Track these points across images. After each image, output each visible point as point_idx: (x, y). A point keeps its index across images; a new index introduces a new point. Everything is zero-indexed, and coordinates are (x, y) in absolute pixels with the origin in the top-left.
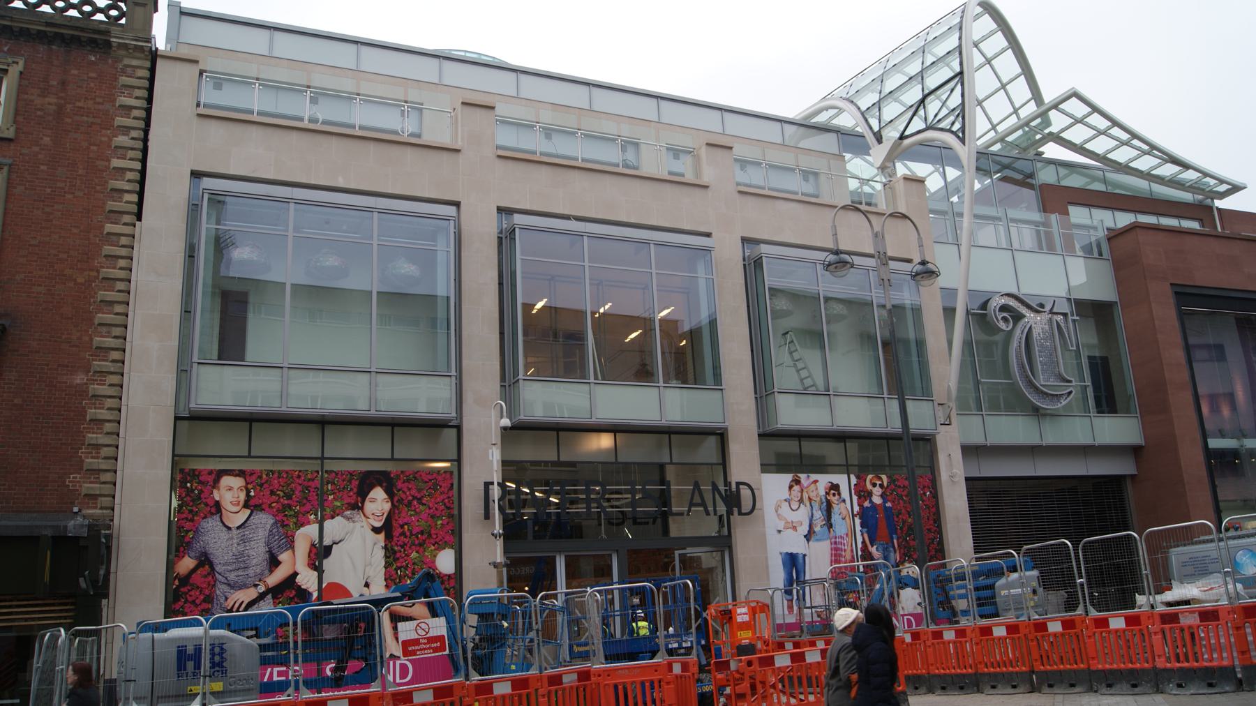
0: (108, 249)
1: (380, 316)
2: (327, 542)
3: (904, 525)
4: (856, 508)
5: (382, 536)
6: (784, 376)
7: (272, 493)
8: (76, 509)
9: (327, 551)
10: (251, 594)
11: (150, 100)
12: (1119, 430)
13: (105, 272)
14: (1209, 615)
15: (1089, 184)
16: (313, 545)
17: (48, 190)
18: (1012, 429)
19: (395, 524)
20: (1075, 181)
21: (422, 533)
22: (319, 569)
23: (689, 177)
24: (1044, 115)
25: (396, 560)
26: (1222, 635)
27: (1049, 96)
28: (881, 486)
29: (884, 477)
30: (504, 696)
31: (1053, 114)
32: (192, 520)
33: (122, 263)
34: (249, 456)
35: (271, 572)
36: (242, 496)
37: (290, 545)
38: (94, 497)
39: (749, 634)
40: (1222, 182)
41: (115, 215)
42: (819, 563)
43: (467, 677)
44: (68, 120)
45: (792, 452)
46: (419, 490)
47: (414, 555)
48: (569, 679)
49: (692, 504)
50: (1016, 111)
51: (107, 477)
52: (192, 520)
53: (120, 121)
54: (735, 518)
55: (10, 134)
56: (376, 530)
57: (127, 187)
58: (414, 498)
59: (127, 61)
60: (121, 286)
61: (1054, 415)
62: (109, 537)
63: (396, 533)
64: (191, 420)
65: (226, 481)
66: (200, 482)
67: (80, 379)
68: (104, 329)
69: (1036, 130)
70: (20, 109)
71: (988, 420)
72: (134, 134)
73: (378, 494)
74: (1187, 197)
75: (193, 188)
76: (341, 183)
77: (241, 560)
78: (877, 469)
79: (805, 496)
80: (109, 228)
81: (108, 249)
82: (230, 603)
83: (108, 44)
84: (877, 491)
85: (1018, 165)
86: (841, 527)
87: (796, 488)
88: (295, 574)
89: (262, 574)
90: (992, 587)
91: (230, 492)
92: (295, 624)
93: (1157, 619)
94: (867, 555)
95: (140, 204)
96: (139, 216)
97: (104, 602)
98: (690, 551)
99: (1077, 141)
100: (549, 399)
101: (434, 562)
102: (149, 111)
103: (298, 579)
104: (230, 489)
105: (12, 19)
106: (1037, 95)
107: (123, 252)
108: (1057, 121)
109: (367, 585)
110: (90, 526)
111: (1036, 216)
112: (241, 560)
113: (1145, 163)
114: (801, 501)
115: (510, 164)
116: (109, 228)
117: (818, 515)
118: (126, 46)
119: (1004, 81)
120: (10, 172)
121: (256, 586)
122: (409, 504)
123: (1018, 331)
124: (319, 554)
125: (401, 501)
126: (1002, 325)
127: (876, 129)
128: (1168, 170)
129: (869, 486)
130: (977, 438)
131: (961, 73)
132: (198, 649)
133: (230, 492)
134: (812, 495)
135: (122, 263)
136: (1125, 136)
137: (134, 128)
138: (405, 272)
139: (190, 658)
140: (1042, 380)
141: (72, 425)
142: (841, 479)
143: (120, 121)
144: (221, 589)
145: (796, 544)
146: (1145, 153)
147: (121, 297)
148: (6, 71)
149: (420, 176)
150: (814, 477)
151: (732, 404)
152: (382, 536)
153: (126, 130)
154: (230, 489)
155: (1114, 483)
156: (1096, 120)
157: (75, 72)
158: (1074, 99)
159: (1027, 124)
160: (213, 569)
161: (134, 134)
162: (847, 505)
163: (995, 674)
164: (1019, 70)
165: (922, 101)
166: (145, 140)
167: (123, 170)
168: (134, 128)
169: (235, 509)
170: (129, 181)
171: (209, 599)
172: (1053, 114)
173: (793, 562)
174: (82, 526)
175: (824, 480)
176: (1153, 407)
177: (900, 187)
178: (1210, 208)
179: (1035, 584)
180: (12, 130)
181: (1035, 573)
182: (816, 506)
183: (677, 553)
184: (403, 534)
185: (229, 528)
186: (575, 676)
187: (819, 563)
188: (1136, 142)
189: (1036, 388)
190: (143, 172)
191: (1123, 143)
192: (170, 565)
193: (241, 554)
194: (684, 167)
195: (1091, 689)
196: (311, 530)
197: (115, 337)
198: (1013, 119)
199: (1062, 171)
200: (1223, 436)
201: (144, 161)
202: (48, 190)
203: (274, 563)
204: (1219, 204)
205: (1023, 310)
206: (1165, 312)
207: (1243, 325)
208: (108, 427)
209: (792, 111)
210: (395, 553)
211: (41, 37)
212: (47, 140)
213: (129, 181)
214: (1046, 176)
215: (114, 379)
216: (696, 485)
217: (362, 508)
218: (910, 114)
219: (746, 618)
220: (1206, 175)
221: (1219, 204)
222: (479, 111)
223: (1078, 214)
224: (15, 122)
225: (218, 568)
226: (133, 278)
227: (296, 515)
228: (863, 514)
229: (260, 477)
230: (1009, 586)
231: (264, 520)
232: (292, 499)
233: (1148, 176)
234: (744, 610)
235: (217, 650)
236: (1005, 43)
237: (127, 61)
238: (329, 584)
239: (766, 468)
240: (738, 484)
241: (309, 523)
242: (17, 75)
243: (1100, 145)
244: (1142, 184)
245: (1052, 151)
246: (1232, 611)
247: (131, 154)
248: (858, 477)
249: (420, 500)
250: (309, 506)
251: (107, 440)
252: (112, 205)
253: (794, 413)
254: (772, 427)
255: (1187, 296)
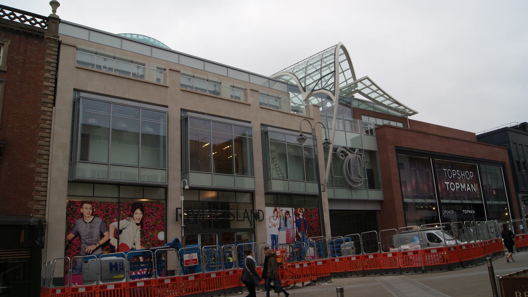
0: (43, 117)
1: (113, 139)
2: (121, 228)
3: (309, 226)
4: (294, 220)
5: (139, 227)
6: (274, 174)
7: (101, 210)
8: (31, 215)
9: (121, 232)
10: (94, 247)
11: (58, 60)
12: (375, 195)
13: (42, 125)
14: (415, 252)
15: (367, 108)
16: (116, 230)
17: (20, 92)
18: (342, 193)
19: (144, 222)
20: (363, 107)
21: (153, 225)
22: (118, 238)
23: (242, 100)
24: (356, 85)
25: (144, 235)
26: (419, 258)
27: (358, 78)
28: (302, 212)
29: (303, 209)
30: (214, 278)
31: (359, 84)
32: (73, 220)
33: (48, 122)
34: (93, 196)
35: (101, 239)
36: (91, 211)
37: (108, 229)
38: (38, 210)
39: (281, 259)
40: (411, 111)
41: (45, 104)
42: (282, 239)
43: (156, 278)
44: (28, 66)
45: (278, 199)
46: (152, 210)
47: (150, 233)
48: (231, 273)
49: (244, 217)
50: (346, 81)
51: (43, 203)
52: (73, 220)
53: (47, 67)
54: (257, 222)
55: (5, 69)
56: (137, 224)
57: (50, 93)
58: (151, 213)
59: (49, 44)
60: (47, 131)
61: (356, 189)
62: (45, 225)
63: (144, 226)
64: (73, 182)
65: (85, 205)
66: (76, 206)
67: (32, 165)
68: (41, 147)
69: (352, 88)
70: (9, 60)
71: (307, 184)
72: (52, 73)
73: (138, 211)
74: (399, 114)
75: (75, 95)
76: (127, 96)
77: (91, 235)
78: (301, 206)
79: (279, 215)
80: (43, 108)
81: (43, 117)
82: (87, 250)
83: (43, 37)
84: (301, 214)
85: (345, 99)
86: (289, 226)
87: (276, 212)
88: (110, 240)
89: (98, 240)
90: (339, 247)
91: (86, 209)
92: (154, 255)
93: (401, 254)
94: (297, 236)
95: (54, 100)
96: (54, 104)
97: (43, 249)
98: (238, 233)
99: (366, 93)
100: (199, 179)
101: (157, 236)
102: (57, 64)
103: (111, 242)
104: (87, 208)
105: (7, 24)
106: (354, 76)
107: (48, 118)
108: (360, 86)
109: (134, 244)
110: (39, 222)
111: (351, 119)
112: (91, 235)
113: (387, 103)
114: (277, 217)
115: (185, 93)
116: (43, 108)
117: (282, 221)
118: (49, 39)
119: (344, 70)
120: (5, 84)
121: (96, 244)
122: (149, 215)
123: (346, 160)
124: (118, 233)
125: (146, 214)
126: (341, 157)
127: (303, 86)
128: (395, 105)
129: (299, 212)
130: (332, 197)
131: (335, 71)
132: (116, 264)
133: (86, 209)
134: (281, 215)
135: (48, 122)
136: (382, 93)
137: (52, 71)
138: (150, 130)
139: (114, 266)
140: (353, 177)
141: (29, 182)
142: (290, 209)
143: (47, 67)
144: (83, 245)
145: (275, 232)
146: (388, 99)
147: (48, 135)
148: (3, 44)
149: (154, 96)
150: (281, 208)
151: (252, 182)
152: (139, 227)
153: (49, 71)
154: (87, 208)
155: (373, 213)
156: (373, 87)
157: (30, 47)
158: (367, 80)
159: (350, 86)
160: (80, 238)
161: (52, 73)
162: (292, 218)
163: (352, 272)
164: (349, 67)
165: (321, 79)
166: (56, 75)
167: (48, 86)
168: (52, 71)
169: (88, 216)
170: (50, 91)
171: (79, 249)
172: (359, 84)
173: (274, 238)
174: (36, 221)
175: (285, 209)
176: (387, 188)
177: (312, 108)
178: (406, 119)
179: (353, 246)
180: (6, 68)
181: (353, 242)
182: (282, 219)
183: (235, 234)
184: (147, 226)
185: (86, 223)
186: (232, 272)
187: (282, 239)
188: (385, 96)
189: (351, 180)
190: (55, 88)
191: (381, 96)
192: (66, 236)
193: (91, 232)
194: (238, 93)
195: (382, 275)
196: (115, 224)
197: (46, 150)
198: (345, 84)
199: (360, 103)
200: (408, 198)
201: (56, 83)
202: (20, 92)
203: (102, 236)
204: (409, 117)
205: (347, 152)
206: (392, 155)
207: (411, 159)
208: (43, 184)
209: (268, 75)
210: (144, 232)
211: (18, 32)
212: (19, 73)
213: (50, 91)
214: (355, 104)
215: (45, 166)
216: (246, 210)
217: (132, 216)
218: (315, 84)
219: (279, 254)
220: (406, 108)
221: (409, 117)
222: (175, 73)
223: (365, 119)
224: (7, 65)
225: (82, 238)
226: (52, 128)
227: (110, 218)
228: (297, 221)
229: (97, 204)
230: (345, 246)
231: (99, 220)
232: (108, 213)
233: (388, 107)
234: (279, 252)
235: (121, 264)
236: (345, 58)
237: (49, 44)
238: (121, 244)
239: (267, 205)
240: (259, 210)
241: (114, 221)
242: (8, 46)
243: (373, 95)
244: (385, 109)
245: (357, 96)
246: (421, 251)
247: (51, 80)
248: (295, 209)
249: (152, 214)
250: (114, 215)
251: (43, 189)
252: (44, 100)
253: (278, 186)
254: (270, 191)
255: (399, 150)
